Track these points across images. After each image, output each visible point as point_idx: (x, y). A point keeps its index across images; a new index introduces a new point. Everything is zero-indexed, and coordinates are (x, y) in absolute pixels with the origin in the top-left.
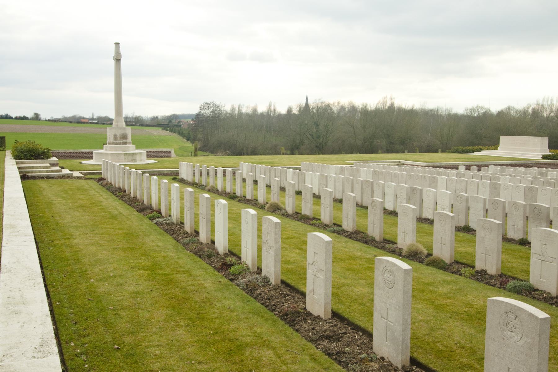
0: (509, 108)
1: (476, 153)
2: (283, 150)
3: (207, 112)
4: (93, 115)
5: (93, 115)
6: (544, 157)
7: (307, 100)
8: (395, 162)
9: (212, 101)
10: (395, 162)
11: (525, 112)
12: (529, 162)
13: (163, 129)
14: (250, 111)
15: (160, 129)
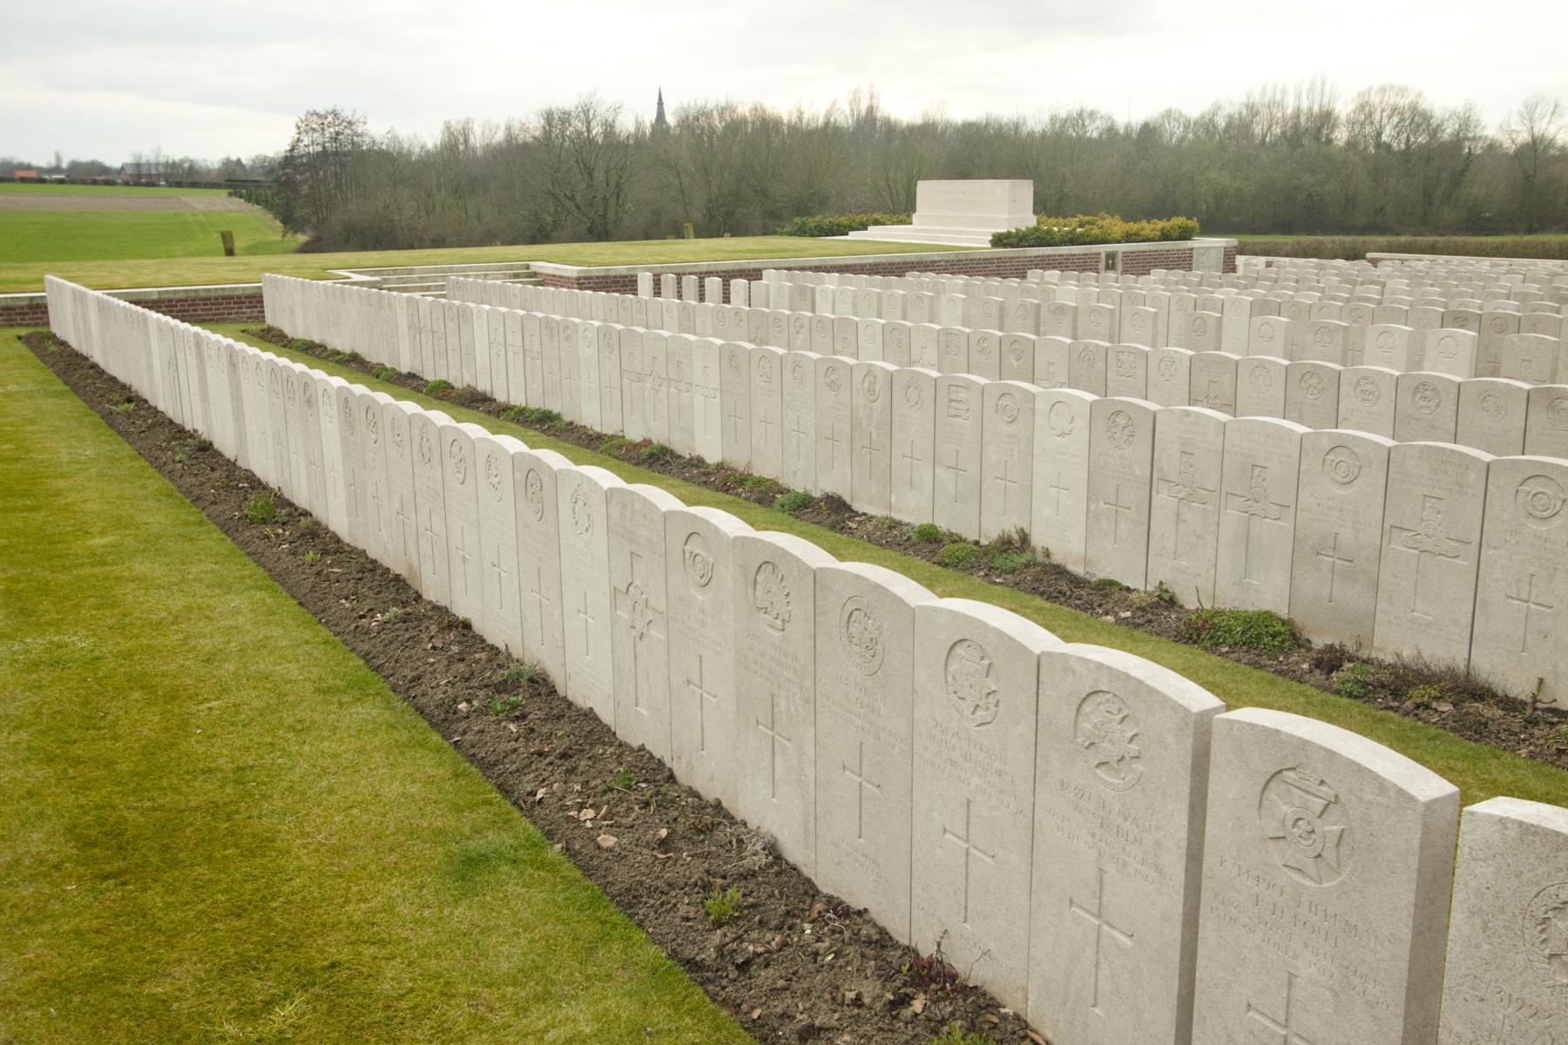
0: (1168, 114)
1: (853, 236)
2: (689, 228)
3: (311, 144)
4: (58, 158)
5: (58, 158)
6: (998, 241)
7: (660, 103)
8: (512, 268)
9: (330, 109)
10: (506, 268)
11: (1207, 126)
12: (935, 256)
13: (230, 194)
14: (500, 136)
15: (224, 193)
